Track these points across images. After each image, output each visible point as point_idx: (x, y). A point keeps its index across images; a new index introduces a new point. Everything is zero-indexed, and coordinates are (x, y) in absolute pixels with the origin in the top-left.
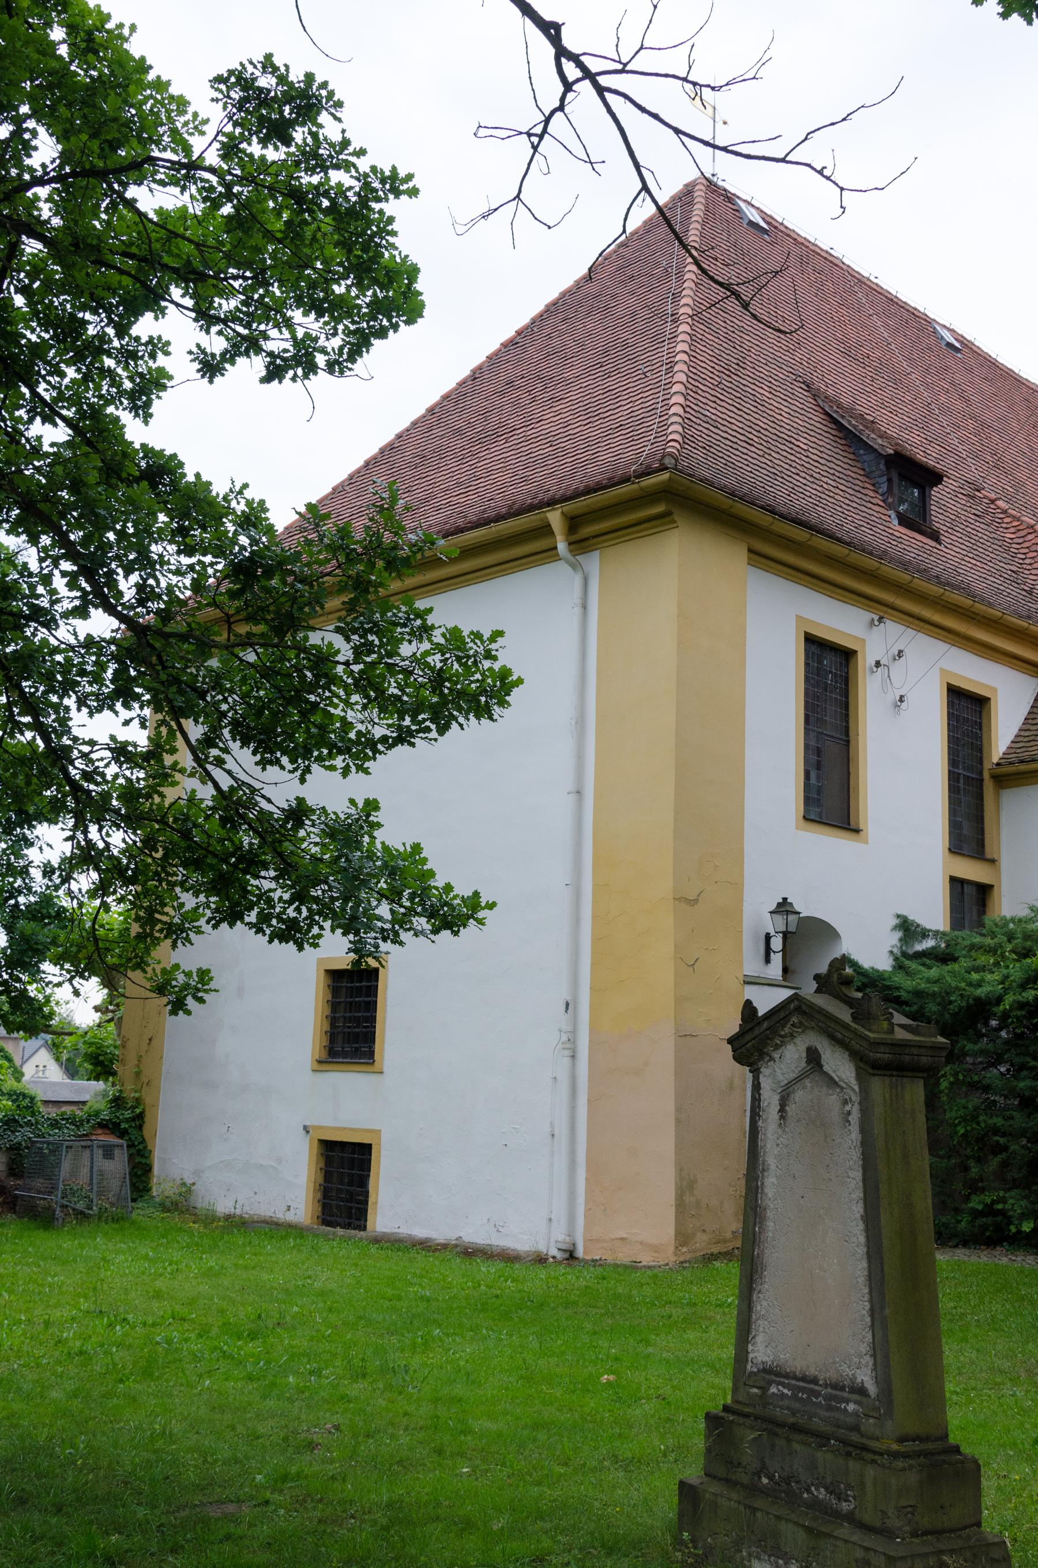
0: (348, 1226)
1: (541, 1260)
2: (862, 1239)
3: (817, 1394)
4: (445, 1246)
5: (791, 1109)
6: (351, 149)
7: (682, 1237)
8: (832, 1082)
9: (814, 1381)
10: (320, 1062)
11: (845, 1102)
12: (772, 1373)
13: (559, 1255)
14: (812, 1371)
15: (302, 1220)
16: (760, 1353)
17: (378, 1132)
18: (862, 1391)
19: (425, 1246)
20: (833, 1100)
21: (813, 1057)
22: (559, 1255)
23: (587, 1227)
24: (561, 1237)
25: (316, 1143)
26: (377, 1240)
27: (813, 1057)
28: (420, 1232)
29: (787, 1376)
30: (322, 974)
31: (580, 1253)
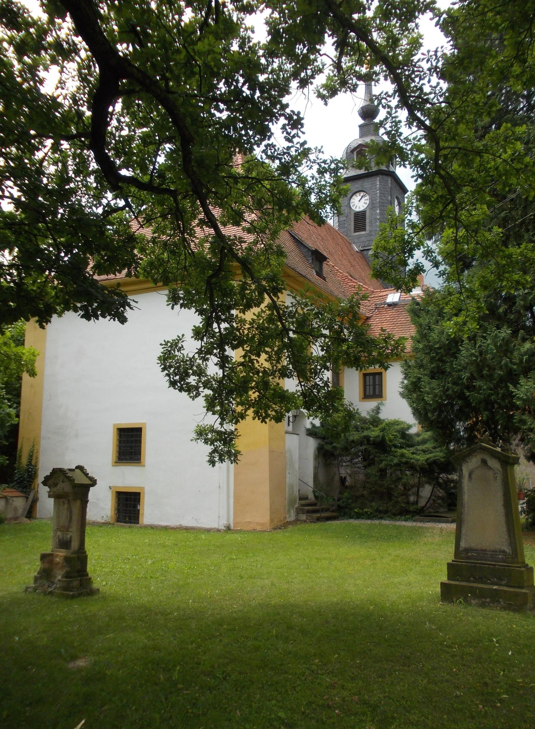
0: (135, 523)
1: (219, 530)
2: (503, 511)
3: (487, 554)
4: (177, 528)
5: (473, 476)
6: (425, 60)
7: (272, 520)
8: (490, 468)
9: (485, 550)
10: (116, 462)
11: (495, 474)
12: (467, 550)
13: (224, 529)
14: (485, 548)
15: (145, 519)
16: (463, 544)
17: (143, 488)
18: (504, 552)
19: (166, 528)
20: (491, 473)
21: (484, 462)
22: (224, 529)
23: (234, 519)
24: (225, 522)
25: (115, 493)
26: (146, 527)
27: (484, 462)
28: (164, 523)
29: (475, 550)
30: (116, 430)
31: (232, 527)
